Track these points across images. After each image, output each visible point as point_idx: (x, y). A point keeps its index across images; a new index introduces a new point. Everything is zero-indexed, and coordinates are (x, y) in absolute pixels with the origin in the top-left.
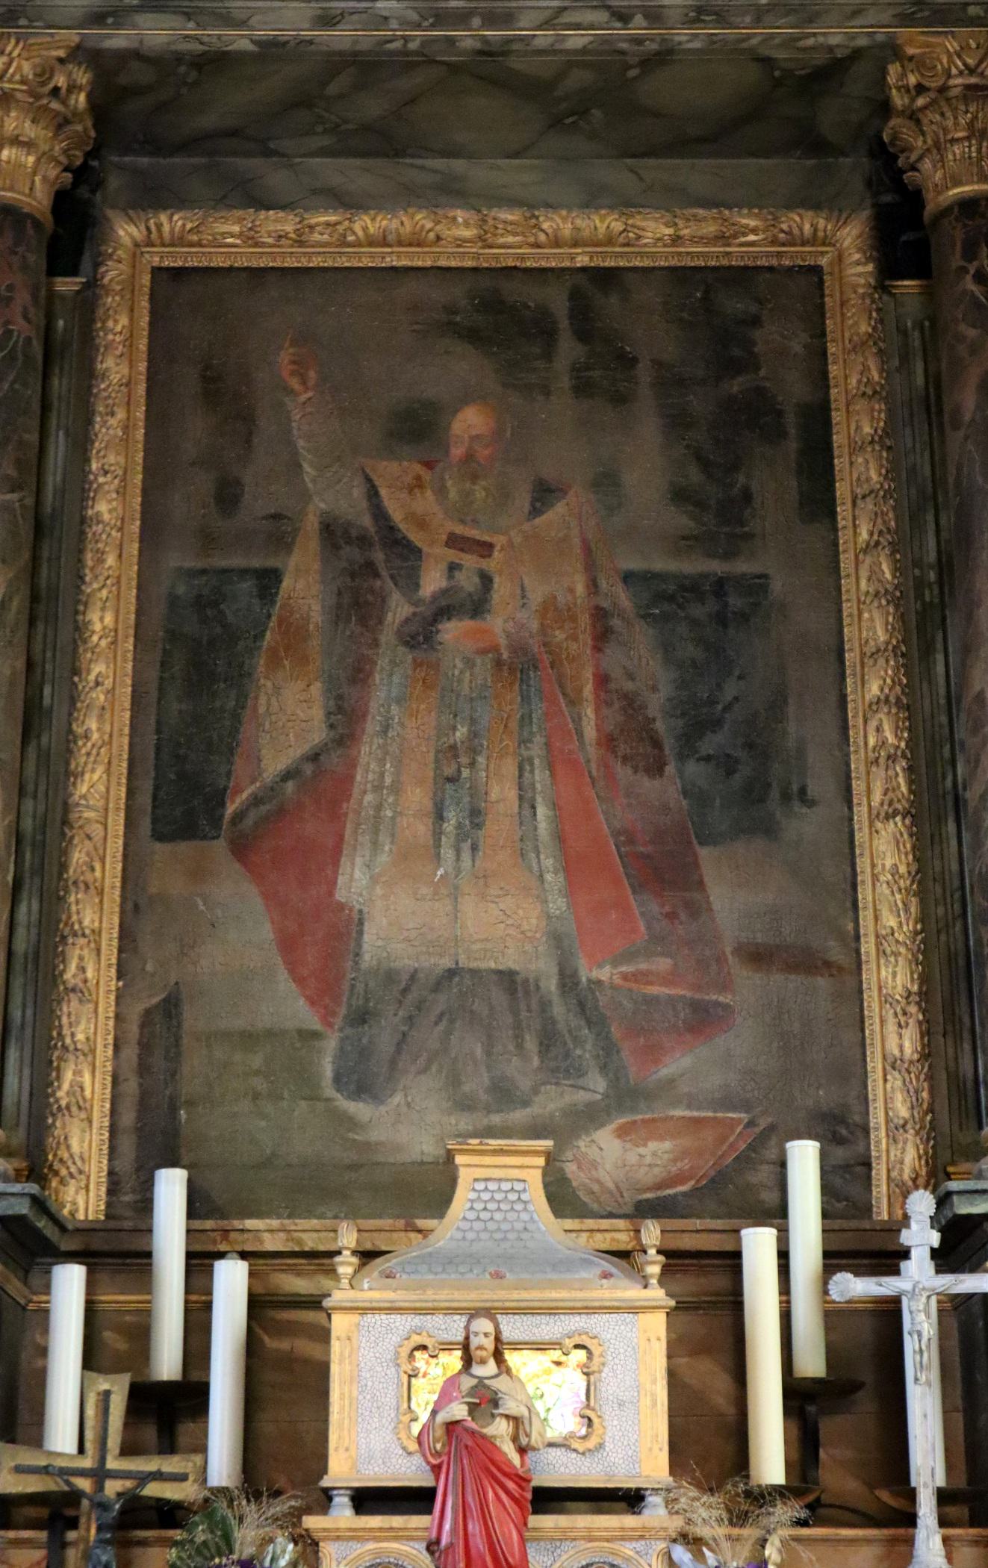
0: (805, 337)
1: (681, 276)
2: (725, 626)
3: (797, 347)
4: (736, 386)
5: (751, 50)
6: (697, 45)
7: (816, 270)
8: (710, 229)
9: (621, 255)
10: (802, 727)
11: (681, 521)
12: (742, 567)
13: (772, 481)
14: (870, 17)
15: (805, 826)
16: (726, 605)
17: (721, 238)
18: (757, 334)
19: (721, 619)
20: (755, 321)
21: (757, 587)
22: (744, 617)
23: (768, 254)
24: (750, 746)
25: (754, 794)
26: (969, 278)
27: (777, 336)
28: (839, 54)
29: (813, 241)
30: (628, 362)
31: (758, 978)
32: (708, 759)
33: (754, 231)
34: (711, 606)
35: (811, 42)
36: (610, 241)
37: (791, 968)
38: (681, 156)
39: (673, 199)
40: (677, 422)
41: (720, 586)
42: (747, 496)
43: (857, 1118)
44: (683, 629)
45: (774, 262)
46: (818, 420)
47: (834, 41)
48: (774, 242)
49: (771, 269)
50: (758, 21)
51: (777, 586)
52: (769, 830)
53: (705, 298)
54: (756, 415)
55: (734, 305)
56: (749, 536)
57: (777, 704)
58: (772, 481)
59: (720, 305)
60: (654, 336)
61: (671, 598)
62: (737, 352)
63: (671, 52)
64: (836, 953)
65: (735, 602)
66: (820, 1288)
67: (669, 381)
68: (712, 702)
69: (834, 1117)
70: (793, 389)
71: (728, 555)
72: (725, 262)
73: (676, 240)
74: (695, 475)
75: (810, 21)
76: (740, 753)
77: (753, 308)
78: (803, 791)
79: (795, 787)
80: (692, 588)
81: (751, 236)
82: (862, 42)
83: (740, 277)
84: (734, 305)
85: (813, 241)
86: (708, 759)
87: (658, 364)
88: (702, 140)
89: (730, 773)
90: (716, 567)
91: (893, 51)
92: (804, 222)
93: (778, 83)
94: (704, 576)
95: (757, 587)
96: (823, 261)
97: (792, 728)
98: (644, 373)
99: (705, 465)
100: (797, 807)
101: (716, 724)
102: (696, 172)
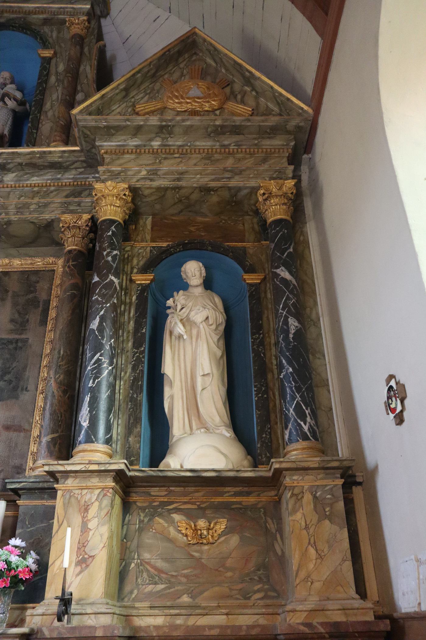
0: (48, 285)
1: (23, 272)
2: (16, 350)
3: (46, 287)
4: (31, 296)
5: (28, 220)
6: (16, 219)
7: (54, 270)
8: (29, 262)
9: (9, 268)
10: (29, 373)
11: (11, 326)
12: (23, 336)
13: (34, 317)
14: (56, 212)
15: (25, 397)
16: (17, 345)
17: (31, 264)
18: (38, 285)
19: (16, 349)
20: (38, 282)
21: (26, 341)
22: (21, 348)
23: (42, 267)
24: (16, 378)
25: (15, 389)
26: (67, 267)
27: (43, 285)
28: (49, 220)
29: (52, 264)
30: (7, 291)
31: (7, 433)
32: (5, 381)
33: (39, 262)
34: (14, 345)
35: (41, 218)
36: (6, 265)
37: (15, 430)
38: (25, 247)
39: (20, 256)
40: (15, 304)
41: (17, 341)
42: (28, 321)
43: (24, 467)
44: (6, 351)
45: (44, 269)
46: (47, 303)
47: (46, 218)
48: (44, 264)
49: (44, 270)
50: (30, 214)
51: (30, 341)
52: (17, 398)
53: (28, 277)
54: (34, 303)
55: (33, 278)
56: (27, 329)
57: (25, 368)
58: (34, 317)
59: (30, 279)
60: (14, 286)
61: (5, 344)
62: (32, 289)
63: (10, 221)
64: (27, 427)
65: (20, 344)
66: (121, 522)
67: (15, 295)
68: (9, 368)
69: (18, 467)
70: (43, 296)
71: (20, 334)
72: (33, 269)
73: (22, 264)
74: (17, 316)
75: (42, 214)
76: (14, 380)
77: (38, 279)
78: (27, 388)
79: (25, 387)
80: (10, 342)
81: (39, 263)
82: (53, 218)
83: (36, 272)
84: (33, 278)
85: (52, 264)
86: (5, 381)
87: (14, 292)
88: (31, 243)
89: (10, 384)
90: (17, 337)
91: (59, 220)
92: (51, 260)
93: (39, 228)
94: (14, 339)
95: (26, 341)
96: (55, 268)
97: (27, 373)
98: (10, 294)
99: (19, 313)
100: (24, 392)
101: (9, 373)
102: (31, 250)
